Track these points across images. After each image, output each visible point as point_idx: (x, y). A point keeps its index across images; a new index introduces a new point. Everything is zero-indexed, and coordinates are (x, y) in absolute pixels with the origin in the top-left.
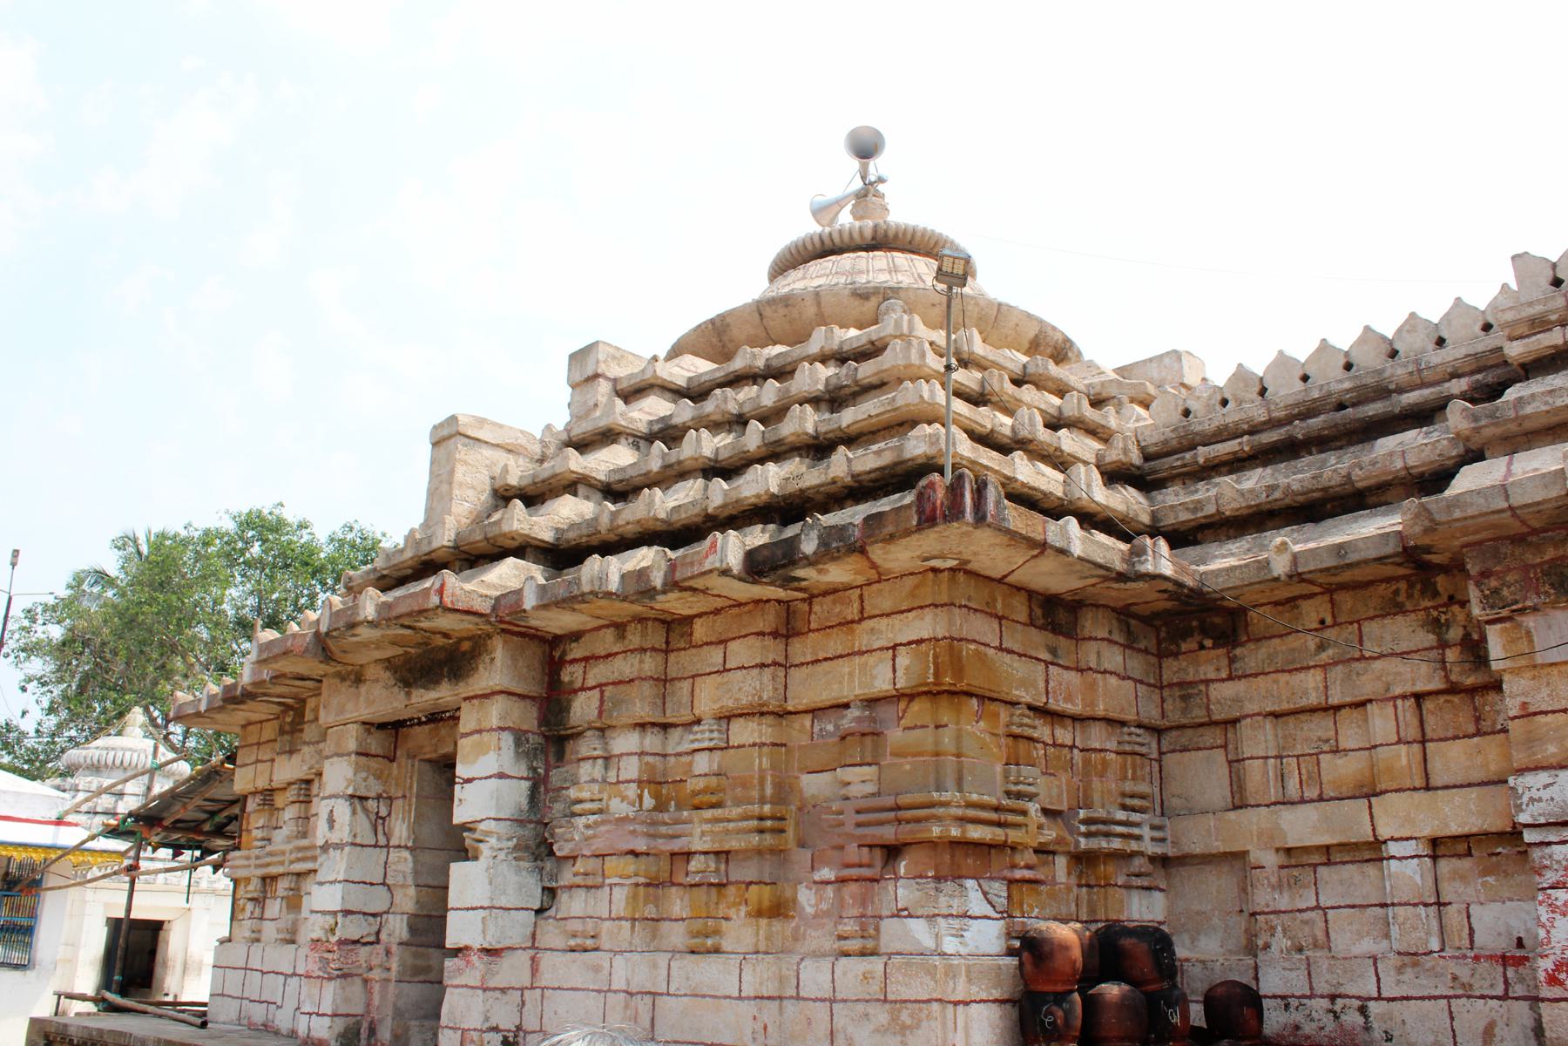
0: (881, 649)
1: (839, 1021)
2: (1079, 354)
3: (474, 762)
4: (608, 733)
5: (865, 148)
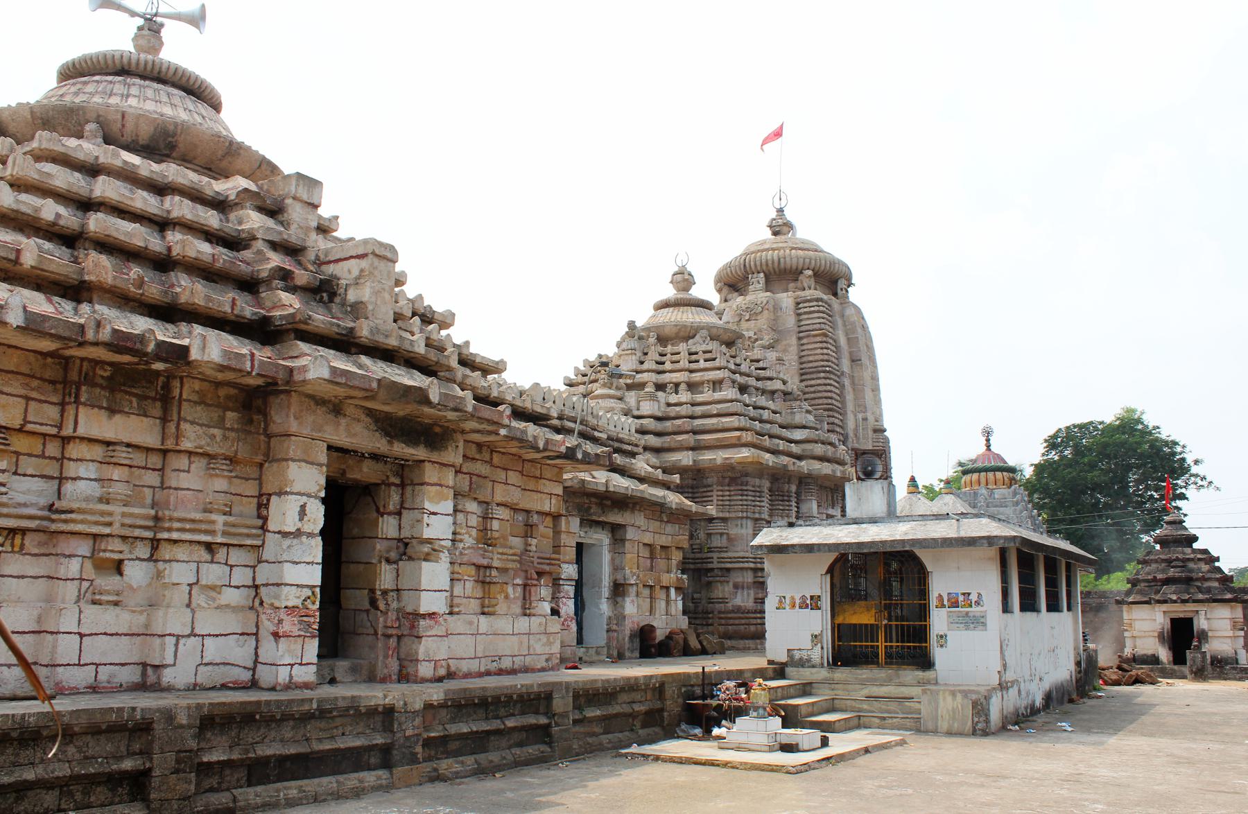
1: (532, 642)
3: (438, 503)
4: (169, 455)
5: (987, 433)
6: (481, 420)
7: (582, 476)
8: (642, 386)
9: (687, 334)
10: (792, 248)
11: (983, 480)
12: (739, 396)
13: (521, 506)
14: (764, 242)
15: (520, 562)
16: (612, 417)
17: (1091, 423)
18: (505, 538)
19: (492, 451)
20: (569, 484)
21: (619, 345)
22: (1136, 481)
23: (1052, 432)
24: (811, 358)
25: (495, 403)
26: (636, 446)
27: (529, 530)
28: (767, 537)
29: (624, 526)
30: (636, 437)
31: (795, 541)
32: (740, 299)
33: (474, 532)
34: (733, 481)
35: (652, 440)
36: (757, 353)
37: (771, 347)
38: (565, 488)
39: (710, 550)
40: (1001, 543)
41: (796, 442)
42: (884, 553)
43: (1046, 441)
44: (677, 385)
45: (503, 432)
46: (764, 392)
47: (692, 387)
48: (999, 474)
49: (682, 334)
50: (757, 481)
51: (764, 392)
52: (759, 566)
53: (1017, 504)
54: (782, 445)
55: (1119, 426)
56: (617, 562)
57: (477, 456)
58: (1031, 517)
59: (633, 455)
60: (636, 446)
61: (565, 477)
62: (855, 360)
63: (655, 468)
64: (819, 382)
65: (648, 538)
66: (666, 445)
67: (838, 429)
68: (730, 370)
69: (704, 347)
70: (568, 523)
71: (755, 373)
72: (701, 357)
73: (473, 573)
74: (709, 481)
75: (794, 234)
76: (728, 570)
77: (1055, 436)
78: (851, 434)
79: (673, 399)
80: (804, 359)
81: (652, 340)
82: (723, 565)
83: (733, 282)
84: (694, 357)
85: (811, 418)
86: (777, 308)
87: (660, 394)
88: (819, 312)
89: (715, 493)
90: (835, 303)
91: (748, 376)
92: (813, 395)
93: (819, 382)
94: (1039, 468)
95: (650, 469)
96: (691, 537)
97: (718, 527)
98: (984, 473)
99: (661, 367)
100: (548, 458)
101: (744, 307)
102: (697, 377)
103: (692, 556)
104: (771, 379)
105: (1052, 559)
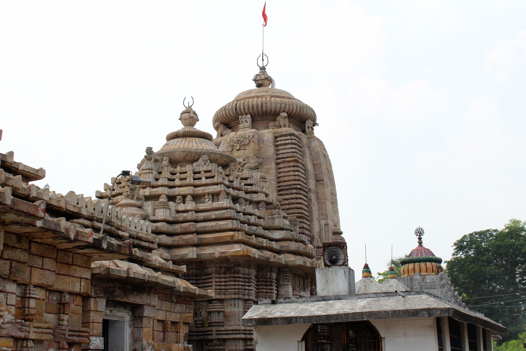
0: (77, 277)
2: (346, 261)
5: (420, 233)
6: (19, 212)
7: (106, 263)
8: (156, 197)
9: (192, 158)
10: (272, 96)
11: (417, 269)
12: (232, 205)
13: (55, 287)
14: (251, 91)
15: (53, 335)
16: (132, 220)
17: (488, 231)
18: (40, 314)
19: (30, 242)
20: (97, 271)
21: (139, 167)
22: (520, 273)
23: (459, 238)
24: (286, 179)
25: (34, 200)
26: (152, 243)
27: (62, 307)
28: (255, 312)
29: (142, 305)
30: (151, 237)
31: (278, 315)
32: (233, 134)
33: (13, 310)
34: (228, 270)
35: (164, 239)
36: (246, 173)
37: (256, 168)
38: (93, 275)
39: (210, 324)
40: (438, 314)
41: (276, 240)
42: (347, 323)
43: (455, 244)
44: (184, 197)
45: (39, 223)
46: (251, 202)
47: (196, 198)
48: (429, 264)
49: (188, 158)
50: (247, 270)
51: (251, 202)
52: (248, 336)
53: (443, 286)
54: (265, 243)
55: (508, 233)
56: (136, 335)
57: (17, 245)
58: (454, 296)
59: (150, 250)
60: (152, 243)
61: (93, 265)
62: (318, 180)
63: (167, 260)
64: (292, 196)
65: (161, 316)
66: (176, 243)
67: (307, 232)
68: (225, 185)
69: (205, 168)
70: (96, 303)
71: (244, 188)
72: (203, 175)
73: (12, 344)
74: (210, 270)
75: (273, 86)
76: (225, 340)
77: (462, 241)
78: (316, 236)
79: (182, 207)
80: (281, 179)
81: (165, 163)
82: (220, 337)
83: (227, 121)
84: (197, 176)
85: (287, 222)
86: (260, 141)
87: (171, 203)
88: (292, 144)
89: (214, 280)
90: (304, 138)
91: (239, 190)
92: (287, 207)
93: (292, 196)
94: (451, 264)
95: (163, 261)
96: (195, 314)
97: (217, 306)
98: (420, 260)
99: (172, 183)
100: (79, 247)
101: (235, 140)
102: (200, 190)
103: (196, 329)
104: (256, 192)
105: (473, 325)
